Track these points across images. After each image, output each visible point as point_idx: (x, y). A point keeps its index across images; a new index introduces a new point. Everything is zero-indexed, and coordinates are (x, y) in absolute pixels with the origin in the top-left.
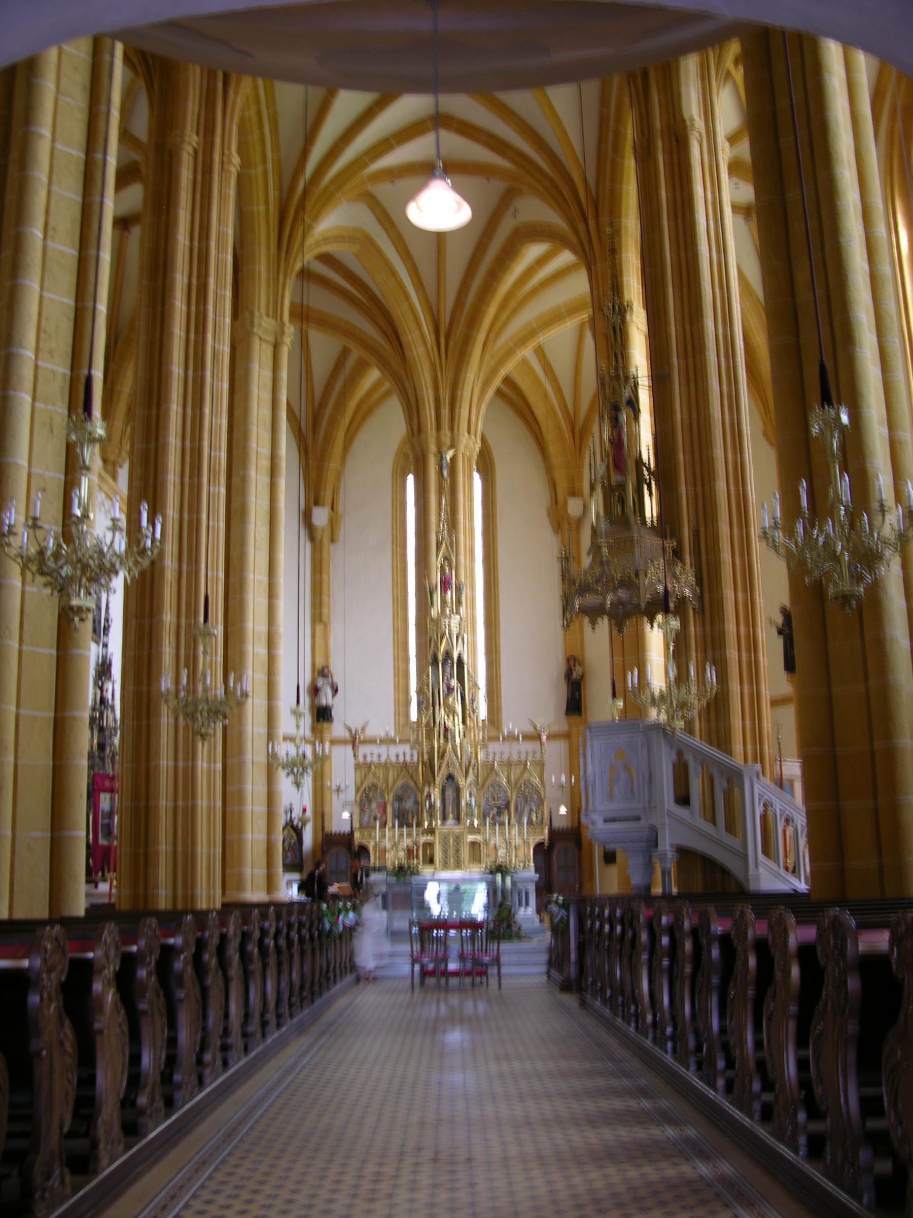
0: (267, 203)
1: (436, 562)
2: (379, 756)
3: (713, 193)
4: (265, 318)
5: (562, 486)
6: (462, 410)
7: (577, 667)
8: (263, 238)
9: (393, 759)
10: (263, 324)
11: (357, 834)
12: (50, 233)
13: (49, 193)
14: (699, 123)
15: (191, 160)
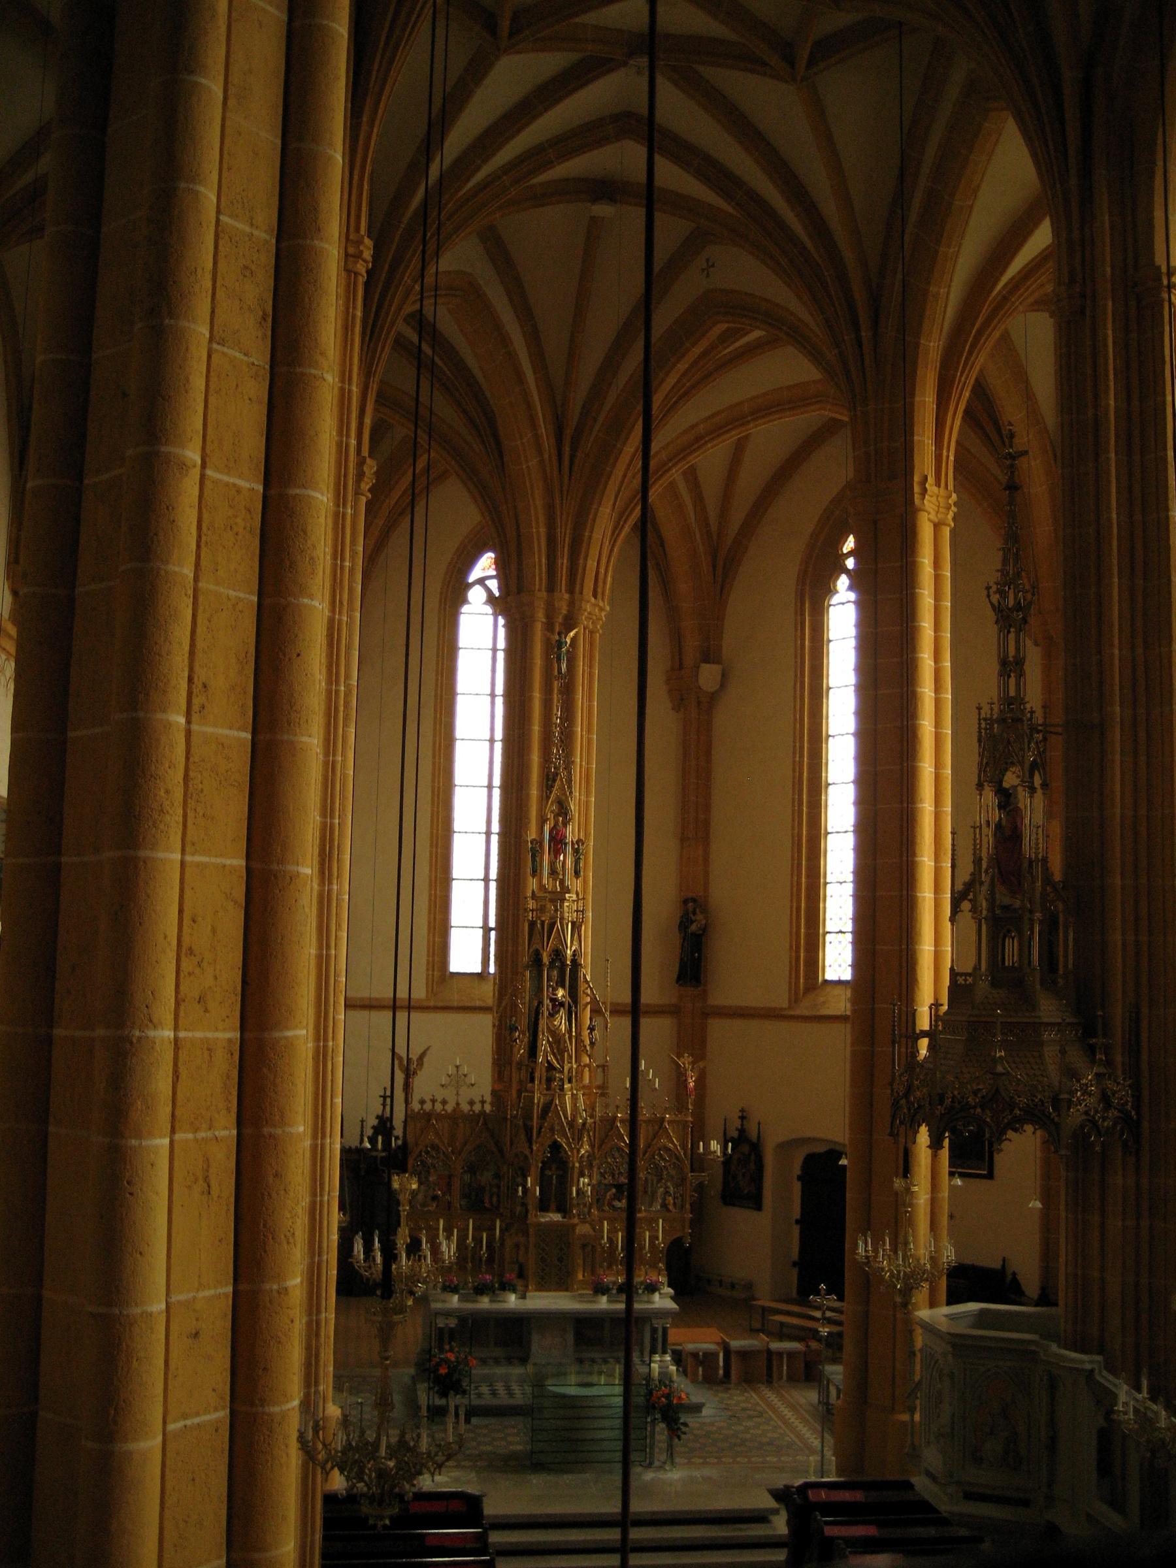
2: (444, 1102)
5: (692, 644)
6: (589, 562)
7: (700, 917)
9: (465, 1107)
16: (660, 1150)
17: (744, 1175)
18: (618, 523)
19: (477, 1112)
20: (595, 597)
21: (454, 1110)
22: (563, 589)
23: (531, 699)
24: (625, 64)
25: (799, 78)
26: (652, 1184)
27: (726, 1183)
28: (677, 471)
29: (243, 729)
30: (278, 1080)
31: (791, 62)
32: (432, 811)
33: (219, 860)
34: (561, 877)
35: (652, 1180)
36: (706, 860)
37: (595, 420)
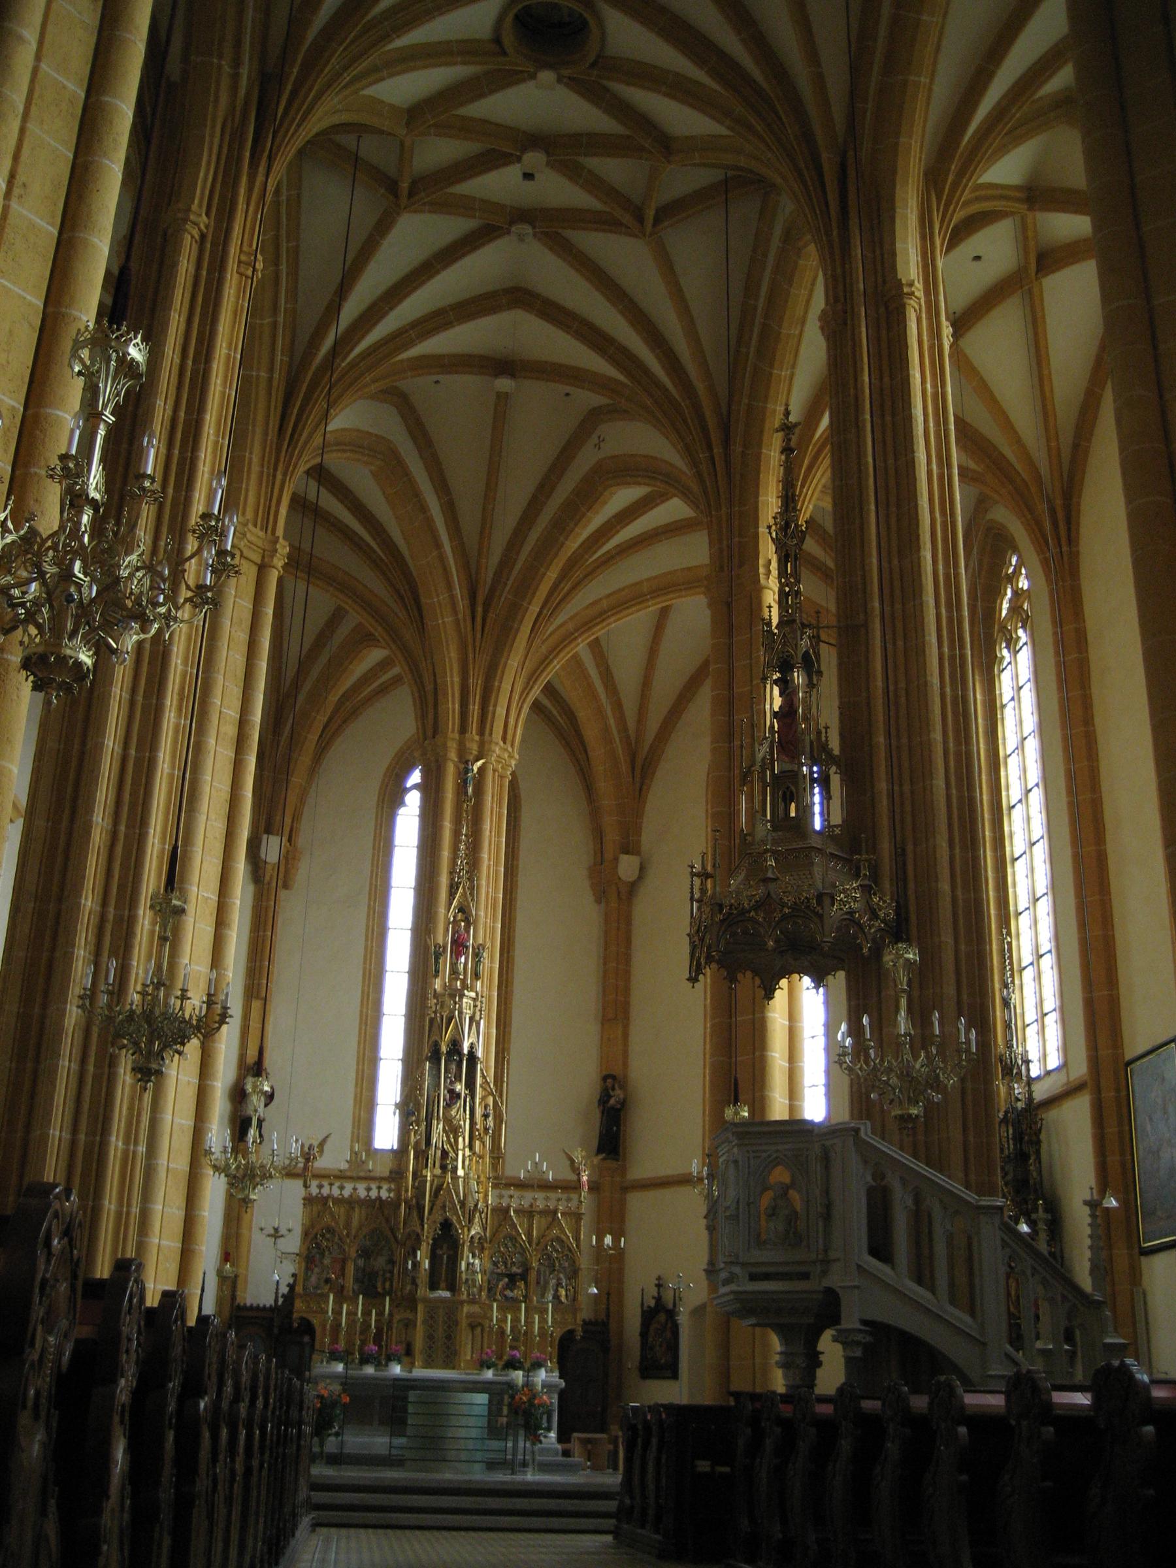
0: (271, 370)
1: (445, 913)
3: (934, 386)
4: (250, 526)
5: (612, 836)
6: (498, 709)
8: (260, 417)
10: (248, 535)
11: (299, 1304)
12: (16, 191)
13: (22, 130)
14: (919, 289)
15: (195, 247)
16: (552, 1241)
17: (661, 1346)
18: (528, 683)
19: (373, 1197)
20: (505, 743)
21: (351, 1196)
22: (474, 732)
23: (441, 827)
24: (509, 233)
25: (648, 233)
26: (545, 1276)
27: (643, 1358)
28: (583, 641)
29: (52, 225)
30: (47, 440)
31: (640, 219)
32: (363, 992)
33: (22, 293)
34: (461, 977)
35: (545, 1272)
36: (626, 1035)
37: (506, 584)
